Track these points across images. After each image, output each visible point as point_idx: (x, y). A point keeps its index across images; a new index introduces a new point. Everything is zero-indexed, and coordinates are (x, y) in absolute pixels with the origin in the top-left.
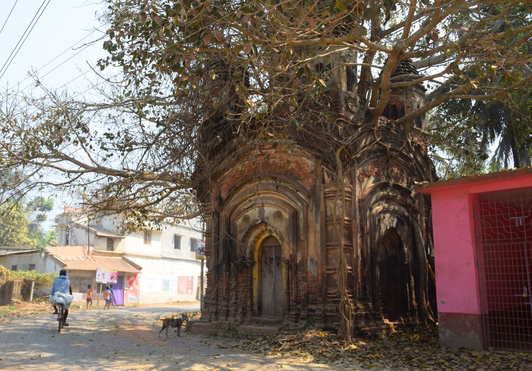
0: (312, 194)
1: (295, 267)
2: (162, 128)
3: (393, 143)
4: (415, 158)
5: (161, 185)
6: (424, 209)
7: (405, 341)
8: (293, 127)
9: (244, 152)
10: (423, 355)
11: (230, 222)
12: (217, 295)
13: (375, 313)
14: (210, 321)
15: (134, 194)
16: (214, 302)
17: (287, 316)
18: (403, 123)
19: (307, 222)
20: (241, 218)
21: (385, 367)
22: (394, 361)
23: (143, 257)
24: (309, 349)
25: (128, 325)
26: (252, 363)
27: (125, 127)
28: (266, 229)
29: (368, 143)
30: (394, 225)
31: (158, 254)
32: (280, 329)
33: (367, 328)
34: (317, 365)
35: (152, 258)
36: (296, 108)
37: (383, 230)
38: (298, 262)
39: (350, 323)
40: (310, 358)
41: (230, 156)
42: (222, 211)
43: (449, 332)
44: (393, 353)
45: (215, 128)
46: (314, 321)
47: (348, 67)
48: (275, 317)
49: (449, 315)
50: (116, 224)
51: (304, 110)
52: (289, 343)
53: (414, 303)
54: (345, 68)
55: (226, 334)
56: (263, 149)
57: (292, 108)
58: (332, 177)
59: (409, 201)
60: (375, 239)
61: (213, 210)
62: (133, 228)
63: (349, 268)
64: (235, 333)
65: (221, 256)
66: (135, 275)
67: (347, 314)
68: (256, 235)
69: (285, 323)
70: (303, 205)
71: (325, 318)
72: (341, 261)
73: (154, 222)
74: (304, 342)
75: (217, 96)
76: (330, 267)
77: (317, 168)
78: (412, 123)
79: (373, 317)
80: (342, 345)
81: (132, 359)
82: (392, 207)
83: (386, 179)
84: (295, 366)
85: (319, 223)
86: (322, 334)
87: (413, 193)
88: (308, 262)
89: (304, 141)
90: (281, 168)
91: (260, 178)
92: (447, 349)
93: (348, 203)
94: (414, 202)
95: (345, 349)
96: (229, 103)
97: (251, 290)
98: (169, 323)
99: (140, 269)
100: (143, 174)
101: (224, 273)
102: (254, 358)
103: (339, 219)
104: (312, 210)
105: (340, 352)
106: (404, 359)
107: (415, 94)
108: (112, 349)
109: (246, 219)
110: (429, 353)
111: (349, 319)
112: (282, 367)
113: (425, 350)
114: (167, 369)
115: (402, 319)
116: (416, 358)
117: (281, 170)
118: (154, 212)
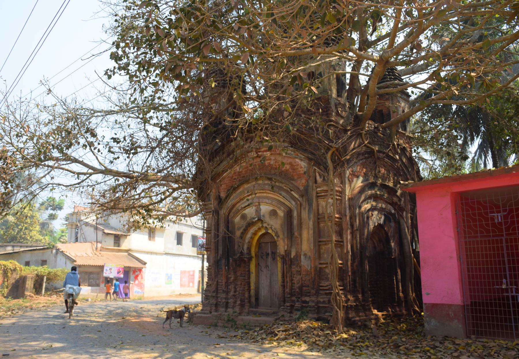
0: (305, 193)
1: (289, 262)
2: (165, 132)
3: (381, 145)
5: (164, 185)
6: (409, 207)
7: (393, 330)
8: (287, 131)
9: (242, 155)
10: (409, 343)
11: (228, 220)
12: (217, 288)
14: (211, 312)
15: (139, 194)
16: (214, 294)
17: (282, 307)
18: (389, 127)
19: (301, 219)
20: (239, 216)
21: (374, 355)
22: (383, 349)
23: (147, 253)
24: (303, 339)
25: (134, 316)
26: (250, 352)
27: (131, 131)
28: (262, 226)
29: (356, 145)
30: (382, 221)
31: (161, 250)
32: (276, 320)
33: (358, 318)
34: (310, 353)
35: (156, 254)
36: (290, 114)
37: (371, 227)
38: (292, 257)
39: (341, 314)
40: (304, 347)
41: (228, 159)
42: (221, 210)
43: (433, 322)
45: (215, 132)
46: (308, 312)
47: (338, 75)
50: (122, 222)
51: (297, 115)
52: (284, 333)
53: (401, 294)
54: (335, 76)
55: (226, 325)
56: (260, 152)
57: (286, 114)
59: (395, 199)
60: (364, 235)
61: (213, 209)
62: (138, 226)
63: (340, 262)
64: (233, 323)
65: (220, 252)
66: (140, 270)
69: (280, 314)
70: (296, 203)
72: (332, 256)
73: (157, 220)
74: (299, 332)
75: (216, 102)
76: (322, 262)
77: (309, 169)
79: (362, 307)
80: (334, 334)
81: (138, 349)
82: (380, 205)
83: (374, 179)
84: (290, 354)
85: (311, 220)
86: (316, 324)
87: (399, 192)
88: (302, 257)
89: (297, 143)
90: (276, 169)
91: (256, 179)
92: (432, 337)
93: (338, 202)
94: (400, 200)
95: (337, 338)
96: (227, 109)
97: (249, 284)
98: (171, 314)
99: (145, 264)
100: (147, 175)
101: (223, 267)
102: (252, 347)
103: (330, 217)
104: (305, 209)
105: (332, 341)
106: (392, 347)
107: (400, 100)
108: (118, 339)
109: (244, 217)
110: (415, 341)
111: (340, 310)
112: (278, 355)
113: (411, 339)
115: (390, 309)
116: (404, 346)
118: (158, 211)
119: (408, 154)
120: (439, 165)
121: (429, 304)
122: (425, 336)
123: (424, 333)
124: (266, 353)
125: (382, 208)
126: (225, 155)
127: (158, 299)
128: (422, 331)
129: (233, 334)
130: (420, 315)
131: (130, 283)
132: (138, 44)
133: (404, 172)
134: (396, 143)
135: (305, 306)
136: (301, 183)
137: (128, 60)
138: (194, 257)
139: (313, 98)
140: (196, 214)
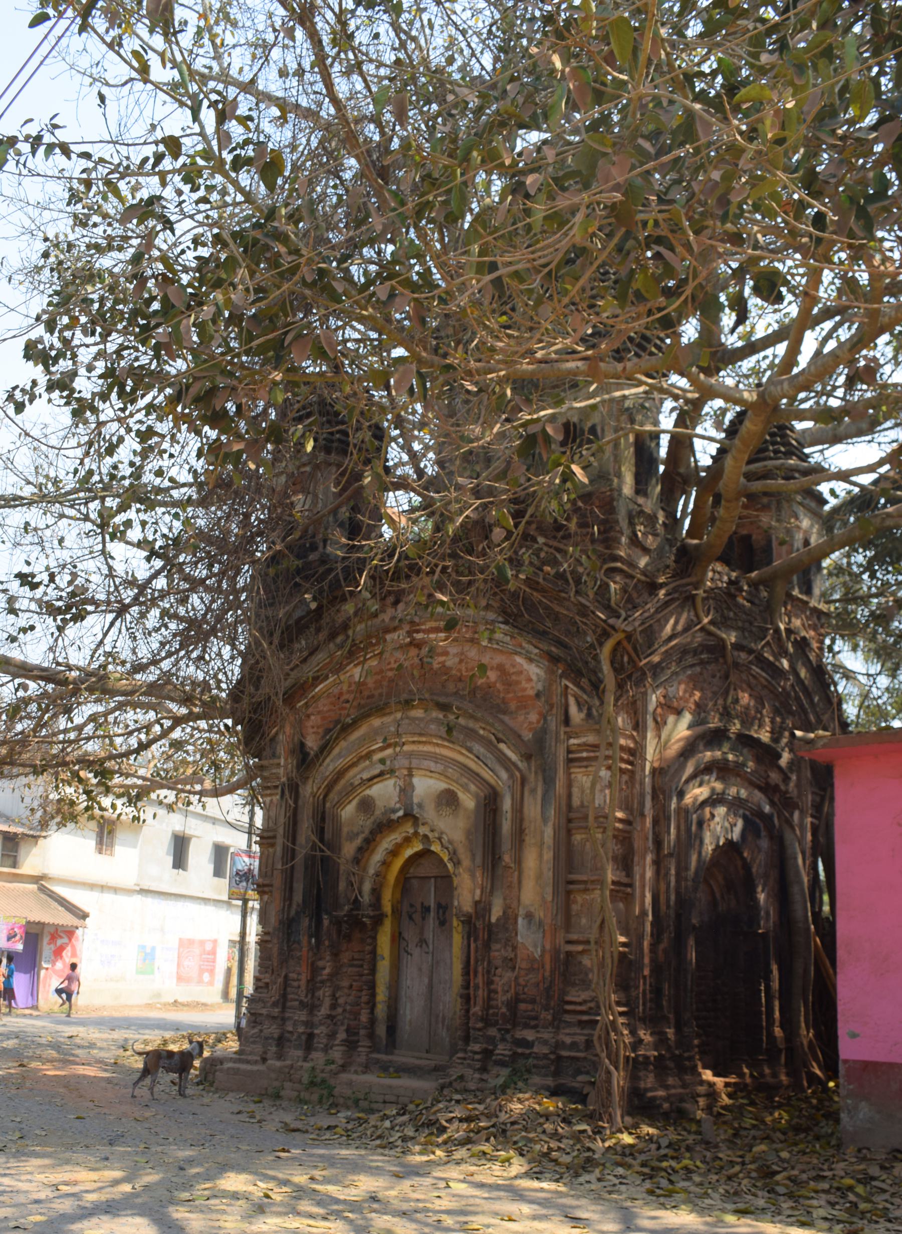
0: (536, 750)
1: (484, 932)
2: (158, 563)
3: (743, 629)
4: (794, 670)
5: (147, 707)
6: (810, 797)
7: (754, 1126)
8: (500, 581)
9: (369, 637)
10: (800, 1166)
11: (324, 812)
12: (284, 996)
13: (681, 1055)
14: (264, 1060)
15: (80, 728)
16: (276, 1011)
17: (460, 1055)
18: (767, 582)
19: (522, 820)
20: (354, 803)
21: (706, 1195)
22: (729, 1178)
23: (92, 886)
24: (515, 1143)
25: (51, 1061)
26: (372, 1174)
27: (65, 555)
28: (416, 834)
29: (680, 628)
30: (736, 835)
31: (130, 882)
32: (442, 1087)
33: (661, 1093)
34: (536, 1184)
35: (115, 890)
36: (509, 534)
37: (709, 847)
38: (493, 919)
39: (619, 1080)
40: (518, 1166)
41: (331, 645)
42: (304, 783)
43: (865, 1110)
44: (725, 1158)
45: (298, 571)
46: (529, 1071)
47: (639, 437)
48: (429, 1056)
49: (869, 1067)
50: (27, 800)
51: (527, 538)
52: (465, 1125)
53: (778, 1031)
54: (631, 438)
55: (304, 1095)
56: (418, 631)
57: (498, 534)
58: (589, 709)
59: (774, 777)
60: (687, 869)
61: (284, 779)
62: (71, 814)
63: (622, 939)
64: (325, 1092)
65: (298, 897)
66: (70, 933)
67: (613, 1057)
68: (390, 847)
69: (454, 1073)
70: (511, 776)
71: (557, 1064)
72: (603, 922)
73: (125, 800)
74: (504, 1124)
75: (305, 491)
76: (574, 937)
77: (550, 685)
78: (791, 582)
79: (674, 1063)
80: (599, 1132)
81: (68, 1155)
82: (733, 791)
83: (720, 720)
84: (481, 1186)
85: (550, 824)
86: (550, 1105)
87: (786, 757)
88: (520, 920)
89: (522, 613)
90: (460, 680)
91: (408, 704)
92: (859, 1151)
93: (625, 777)
94: (786, 779)
95: (607, 1144)
96: (335, 512)
97: (372, 986)
98: (158, 1060)
99: (84, 916)
100: (105, 677)
101: (304, 940)
102: (377, 1159)
103: (603, 817)
104: (533, 791)
105: (594, 1151)
106: (754, 1174)
107: (801, 511)
108: (12, 1125)
109: (366, 805)
110: (815, 1161)
111: (617, 1068)
112: (448, 1187)
113: (805, 1153)
114: (156, 1184)
115: (746, 1070)
116: (784, 1174)
117: (460, 685)
118: (127, 775)
119: (812, 656)
120: (887, 689)
121: (854, 1061)
122: (838, 1146)
123: (839, 1139)
124: (416, 1180)
125: (737, 798)
126: (322, 636)
127: (116, 1014)
128: (832, 1134)
129: (326, 1122)
130: (826, 1089)
131: (41, 968)
132: (102, 322)
133: (801, 706)
134: (782, 627)
135: (522, 1054)
136: (527, 722)
137: (75, 363)
138: (217, 902)
139: (573, 496)
140: (231, 790)
